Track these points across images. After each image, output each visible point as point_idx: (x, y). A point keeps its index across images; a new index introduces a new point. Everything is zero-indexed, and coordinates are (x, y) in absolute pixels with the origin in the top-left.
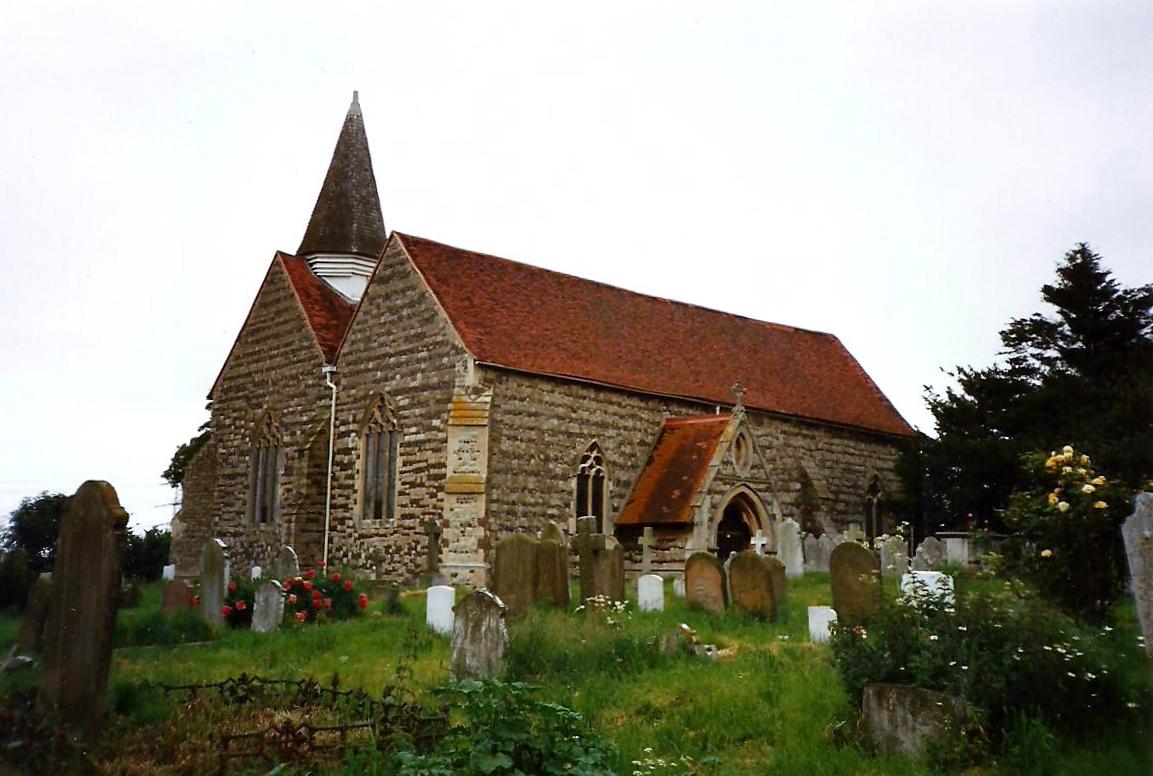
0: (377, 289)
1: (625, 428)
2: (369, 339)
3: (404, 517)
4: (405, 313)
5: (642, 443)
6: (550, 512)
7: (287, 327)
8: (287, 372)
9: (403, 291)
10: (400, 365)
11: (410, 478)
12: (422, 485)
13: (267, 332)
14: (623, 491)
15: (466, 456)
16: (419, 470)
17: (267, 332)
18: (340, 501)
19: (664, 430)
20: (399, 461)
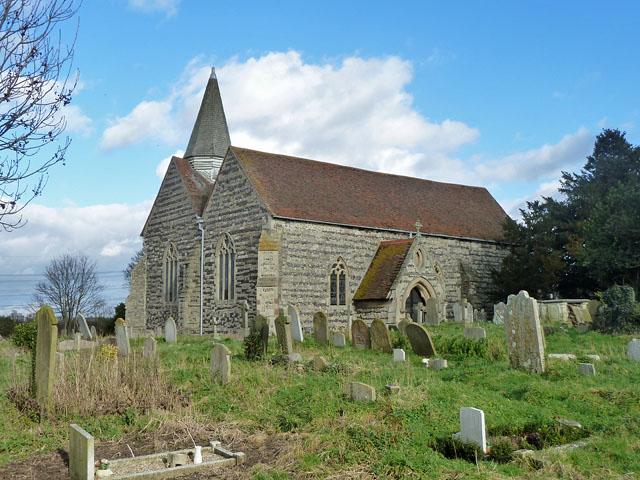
0: (222, 177)
1: (357, 248)
3: (239, 298)
4: (236, 190)
5: (367, 255)
6: (315, 294)
7: (178, 197)
8: (181, 221)
9: (236, 178)
11: (241, 278)
12: (247, 282)
13: (169, 201)
16: (245, 274)
17: (169, 201)
18: (207, 290)
19: (380, 248)
20: (236, 269)
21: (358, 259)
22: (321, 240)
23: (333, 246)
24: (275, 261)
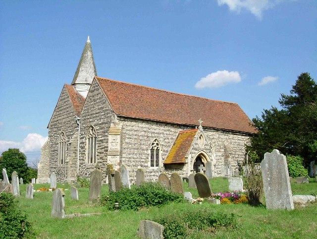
0: (91, 94)
2: (88, 109)
5: (172, 139)
6: (142, 160)
10: (97, 117)
12: (103, 153)
13: (62, 108)
14: (166, 153)
15: (114, 144)
17: (62, 108)
18: (81, 158)
20: (97, 145)
21: (167, 141)
24: (119, 140)
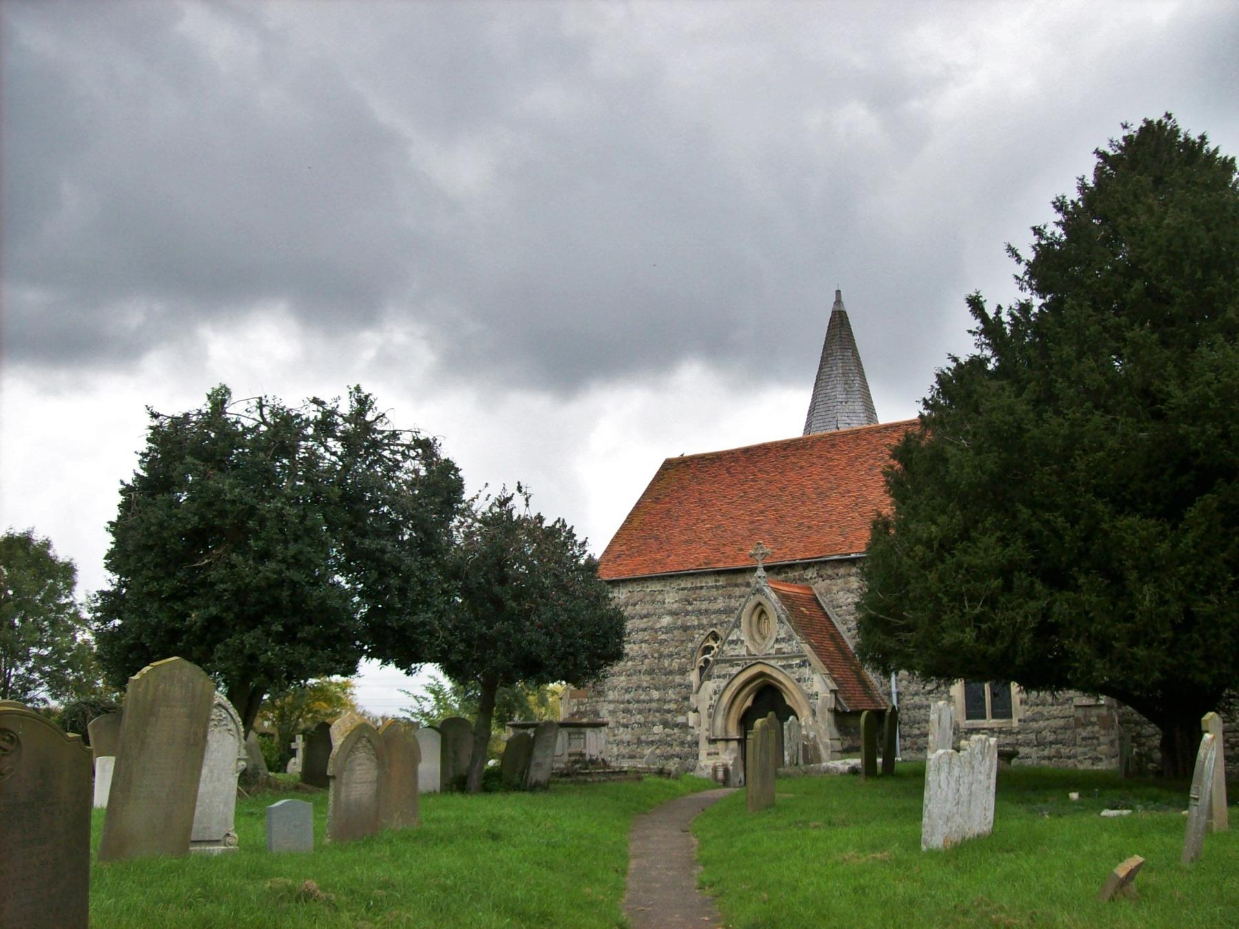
6: (666, 707)
22: (676, 605)
23: (700, 612)
